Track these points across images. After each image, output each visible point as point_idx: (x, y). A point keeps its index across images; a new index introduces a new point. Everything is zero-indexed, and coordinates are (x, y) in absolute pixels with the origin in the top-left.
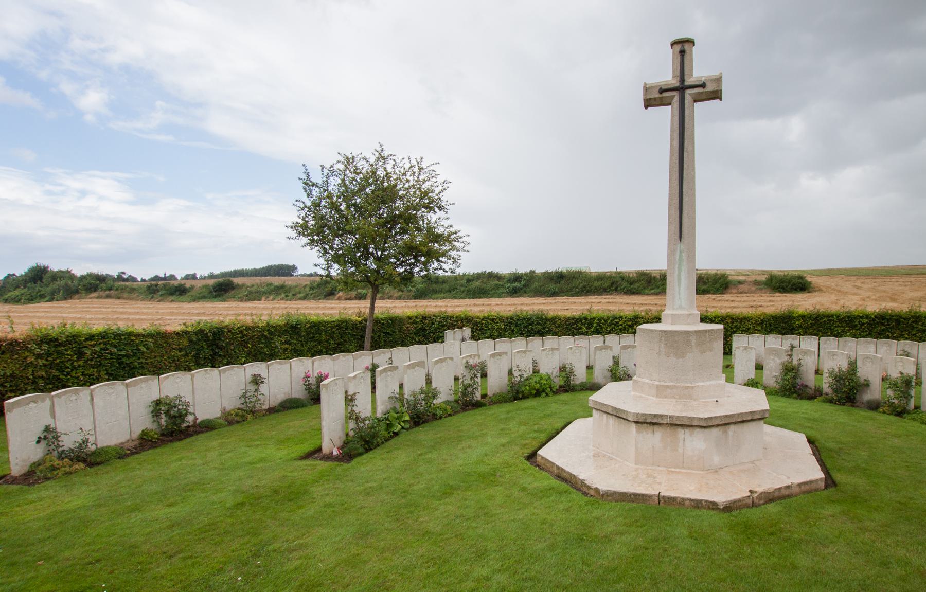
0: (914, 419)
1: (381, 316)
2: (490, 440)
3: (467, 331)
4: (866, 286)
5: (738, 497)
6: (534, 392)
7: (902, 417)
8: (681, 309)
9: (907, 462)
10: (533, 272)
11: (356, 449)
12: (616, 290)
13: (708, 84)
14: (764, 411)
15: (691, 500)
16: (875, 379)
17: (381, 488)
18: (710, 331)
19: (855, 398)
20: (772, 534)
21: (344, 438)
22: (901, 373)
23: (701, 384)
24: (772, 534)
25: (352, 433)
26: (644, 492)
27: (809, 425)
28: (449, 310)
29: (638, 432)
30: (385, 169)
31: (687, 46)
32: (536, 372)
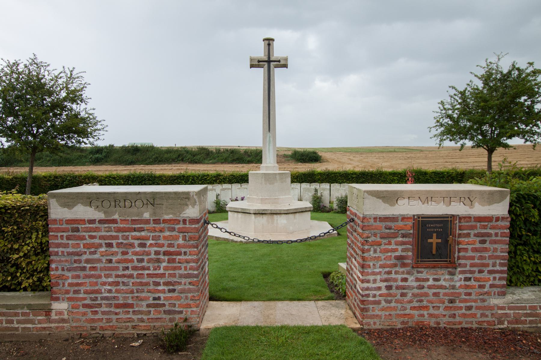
10: (112, 146)
29: (255, 218)
31: (271, 42)
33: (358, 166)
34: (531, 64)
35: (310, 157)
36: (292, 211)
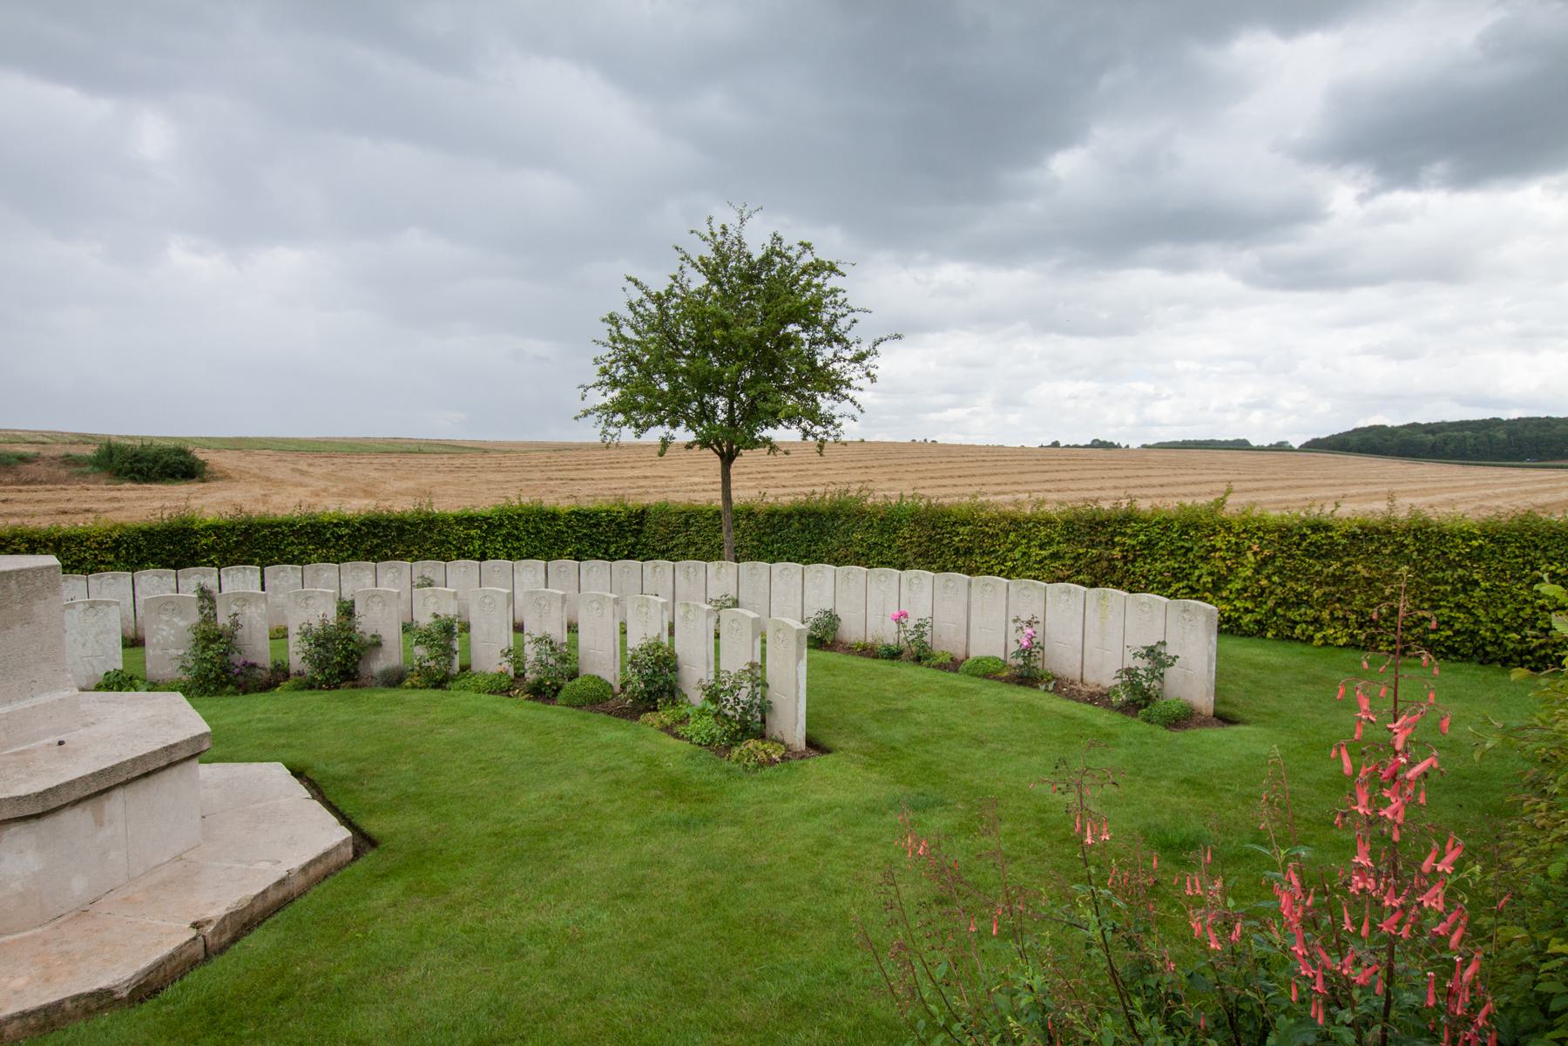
0: (464, 688)
4: (318, 471)
5: (166, 950)
7: (444, 688)
9: (479, 761)
14: (197, 739)
16: (391, 635)
18: (19, 572)
19: (357, 672)
20: (281, 998)
22: (436, 616)
24: (281, 998)
27: (283, 741)
33: (325, 490)
34: (806, 246)
35: (166, 465)
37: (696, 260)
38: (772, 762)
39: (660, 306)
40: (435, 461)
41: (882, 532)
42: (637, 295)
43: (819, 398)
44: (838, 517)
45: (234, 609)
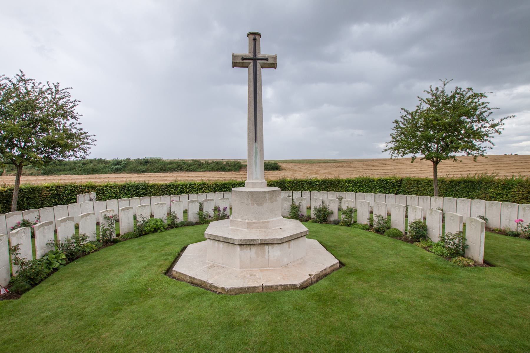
1: (23, 187)
2: (134, 265)
3: (93, 195)
4: (304, 168)
6: (153, 230)
8: (256, 180)
11: (22, 286)
12: (181, 169)
13: (269, 59)
14: (306, 231)
15: (281, 285)
17: (57, 315)
21: (9, 279)
22: (348, 207)
23: (272, 220)
25: (15, 274)
26: (253, 286)
28: (77, 181)
29: (241, 250)
30: (26, 88)
31: (257, 37)
32: (152, 216)
36: (287, 240)
37: (425, 99)
38: (469, 265)
39: (412, 116)
40: (332, 165)
41: (503, 189)
42: (404, 113)
43: (474, 141)
44: (481, 183)
45: (299, 201)
